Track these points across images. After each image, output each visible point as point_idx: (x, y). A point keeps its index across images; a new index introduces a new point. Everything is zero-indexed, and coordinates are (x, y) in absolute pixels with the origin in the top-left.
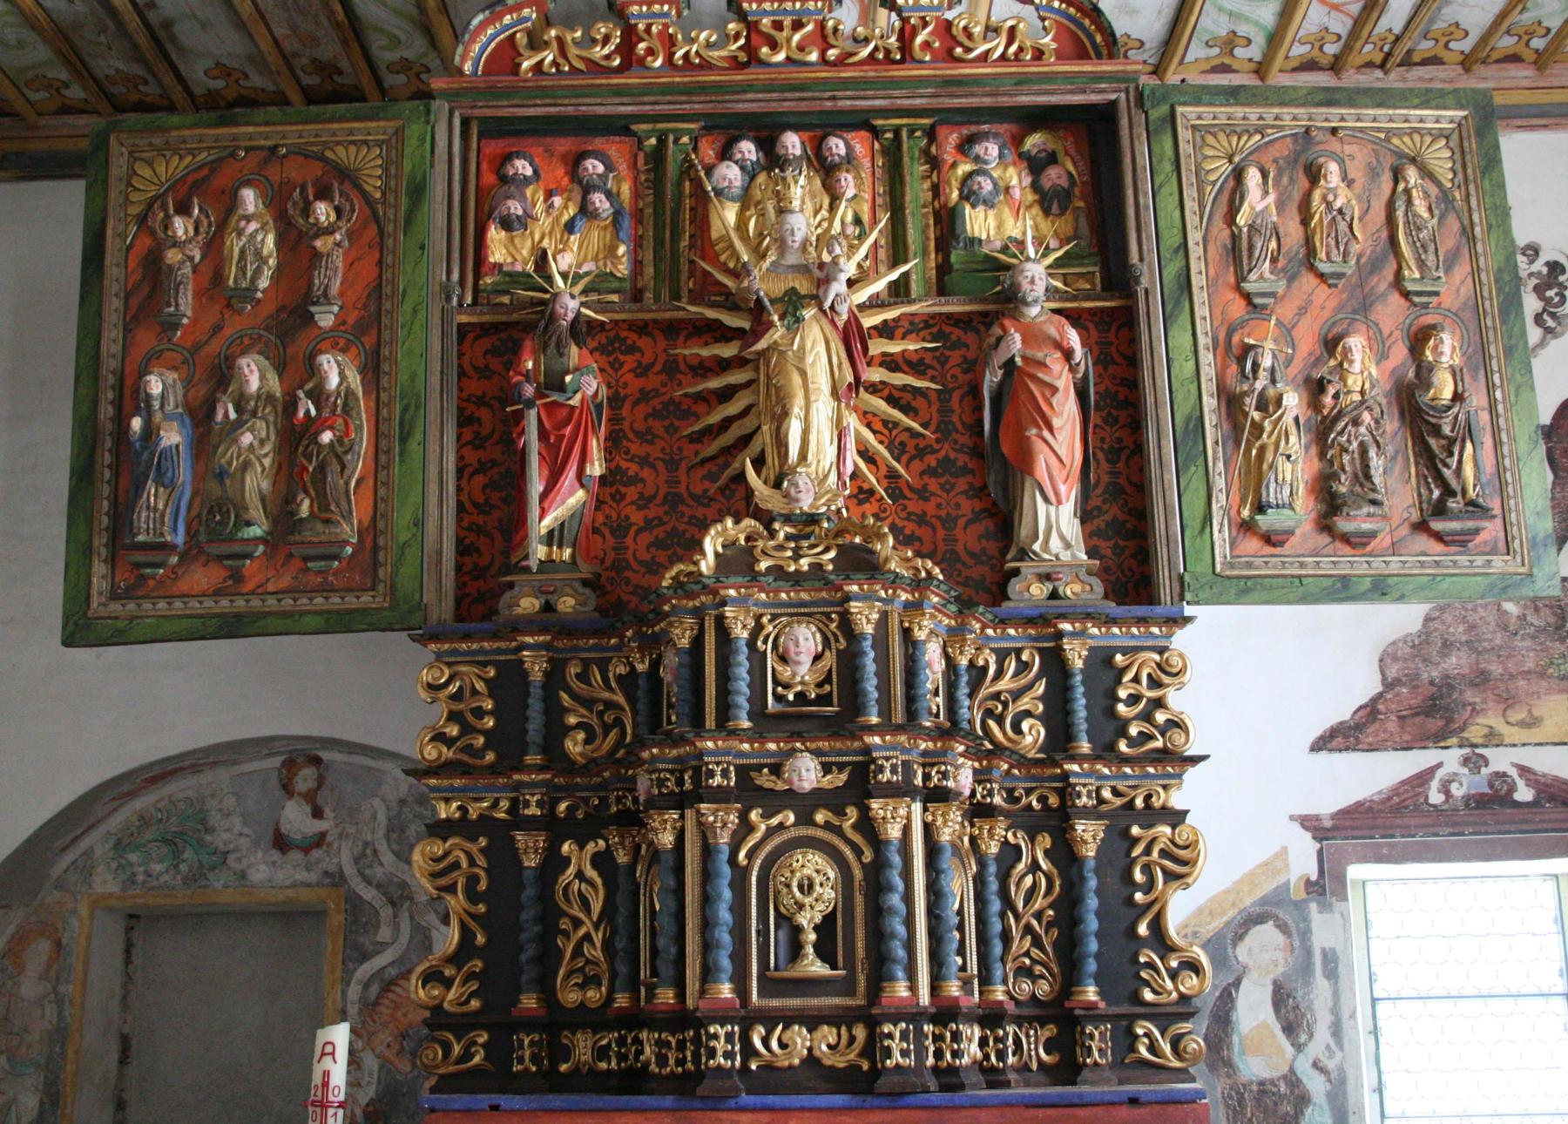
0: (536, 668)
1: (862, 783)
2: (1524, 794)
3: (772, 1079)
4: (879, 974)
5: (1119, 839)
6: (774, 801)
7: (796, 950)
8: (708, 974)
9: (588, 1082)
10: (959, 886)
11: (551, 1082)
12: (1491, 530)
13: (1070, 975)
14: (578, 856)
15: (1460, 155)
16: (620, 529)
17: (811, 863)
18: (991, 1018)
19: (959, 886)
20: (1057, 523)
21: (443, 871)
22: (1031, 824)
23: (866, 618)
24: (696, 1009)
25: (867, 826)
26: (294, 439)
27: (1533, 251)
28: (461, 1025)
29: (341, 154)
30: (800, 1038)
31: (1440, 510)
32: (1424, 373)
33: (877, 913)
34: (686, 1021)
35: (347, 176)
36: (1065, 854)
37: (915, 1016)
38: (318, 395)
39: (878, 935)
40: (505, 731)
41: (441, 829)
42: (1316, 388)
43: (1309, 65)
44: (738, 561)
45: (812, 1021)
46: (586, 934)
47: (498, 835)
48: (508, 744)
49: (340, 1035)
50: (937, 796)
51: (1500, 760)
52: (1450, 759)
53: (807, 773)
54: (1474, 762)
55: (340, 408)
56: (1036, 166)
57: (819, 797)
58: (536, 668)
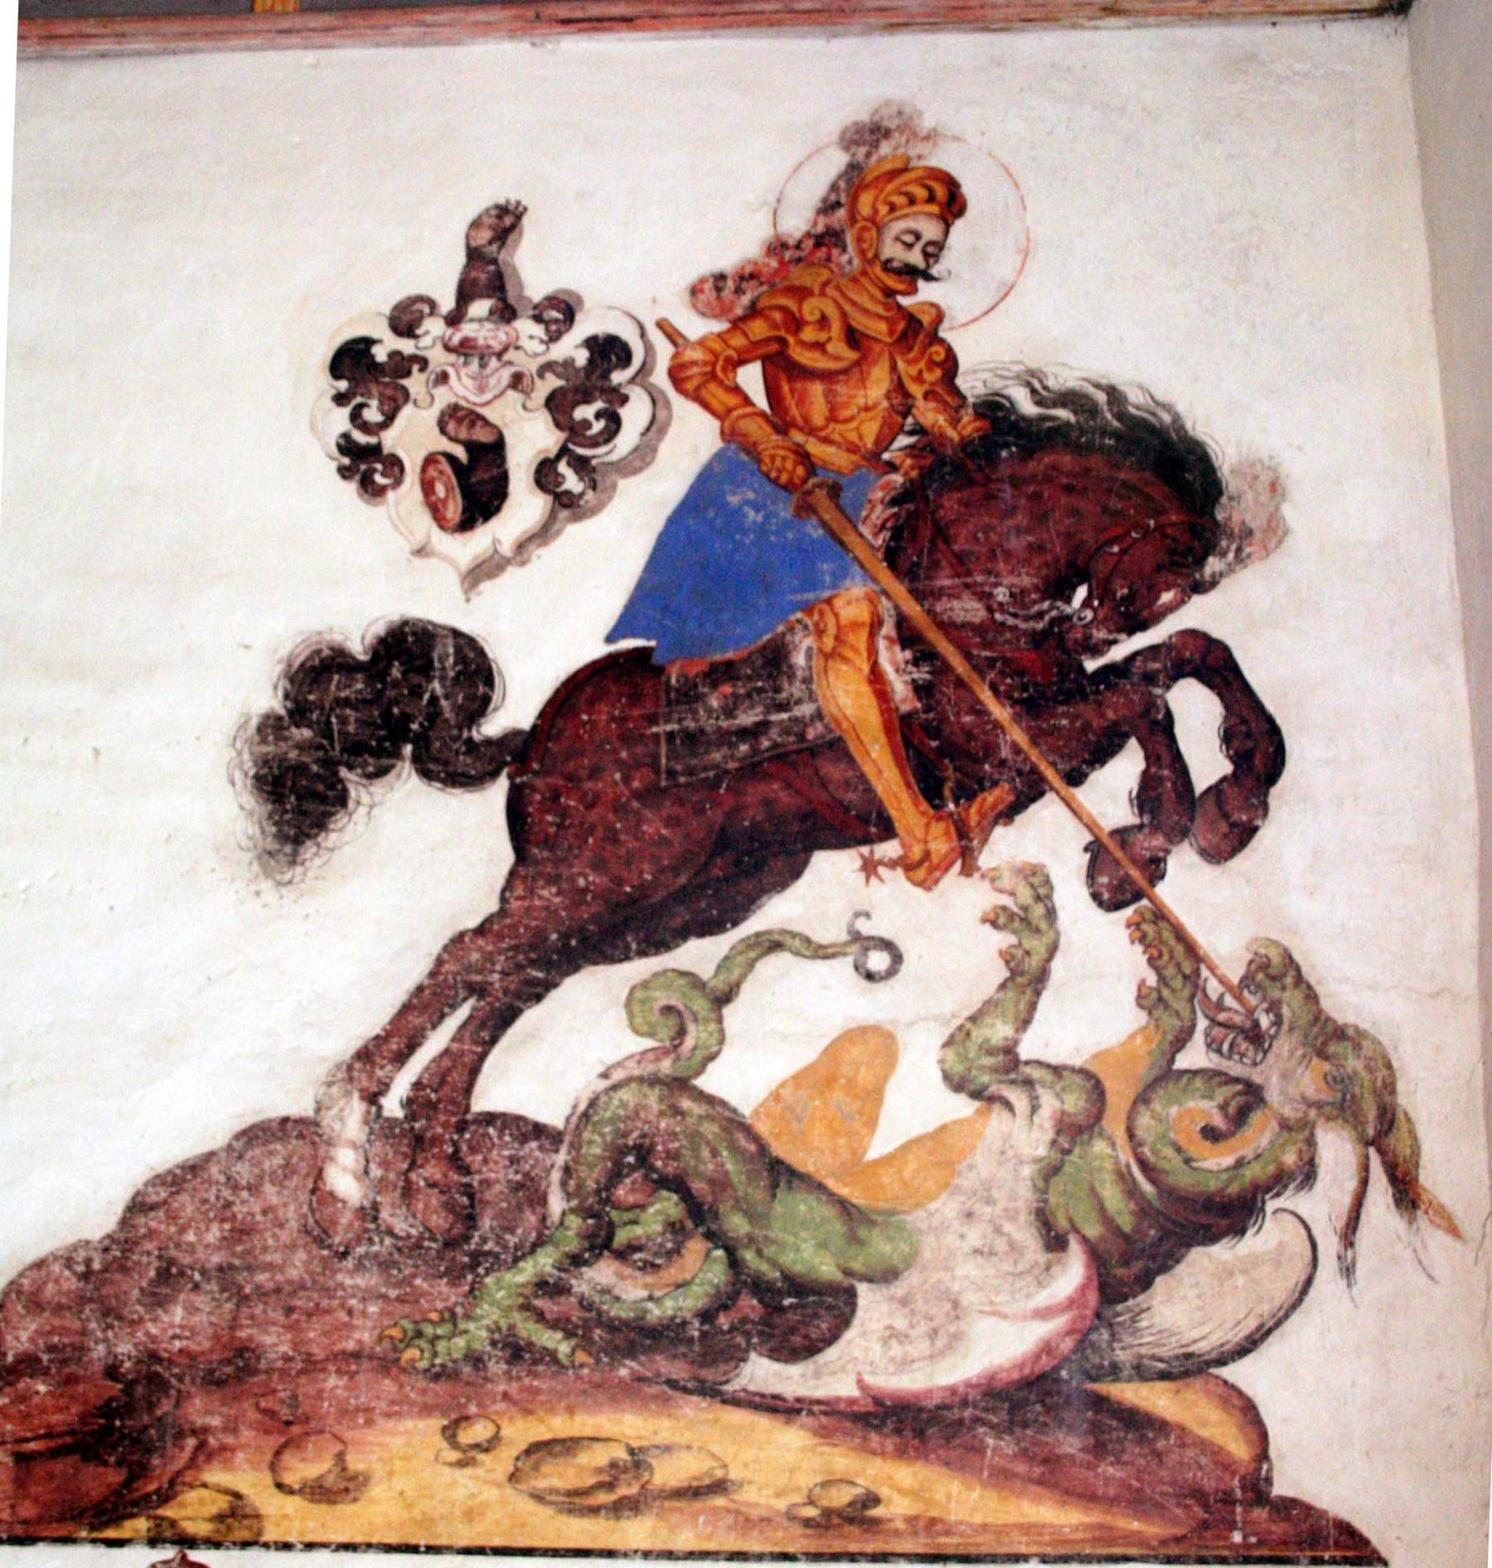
27: (562, 311)
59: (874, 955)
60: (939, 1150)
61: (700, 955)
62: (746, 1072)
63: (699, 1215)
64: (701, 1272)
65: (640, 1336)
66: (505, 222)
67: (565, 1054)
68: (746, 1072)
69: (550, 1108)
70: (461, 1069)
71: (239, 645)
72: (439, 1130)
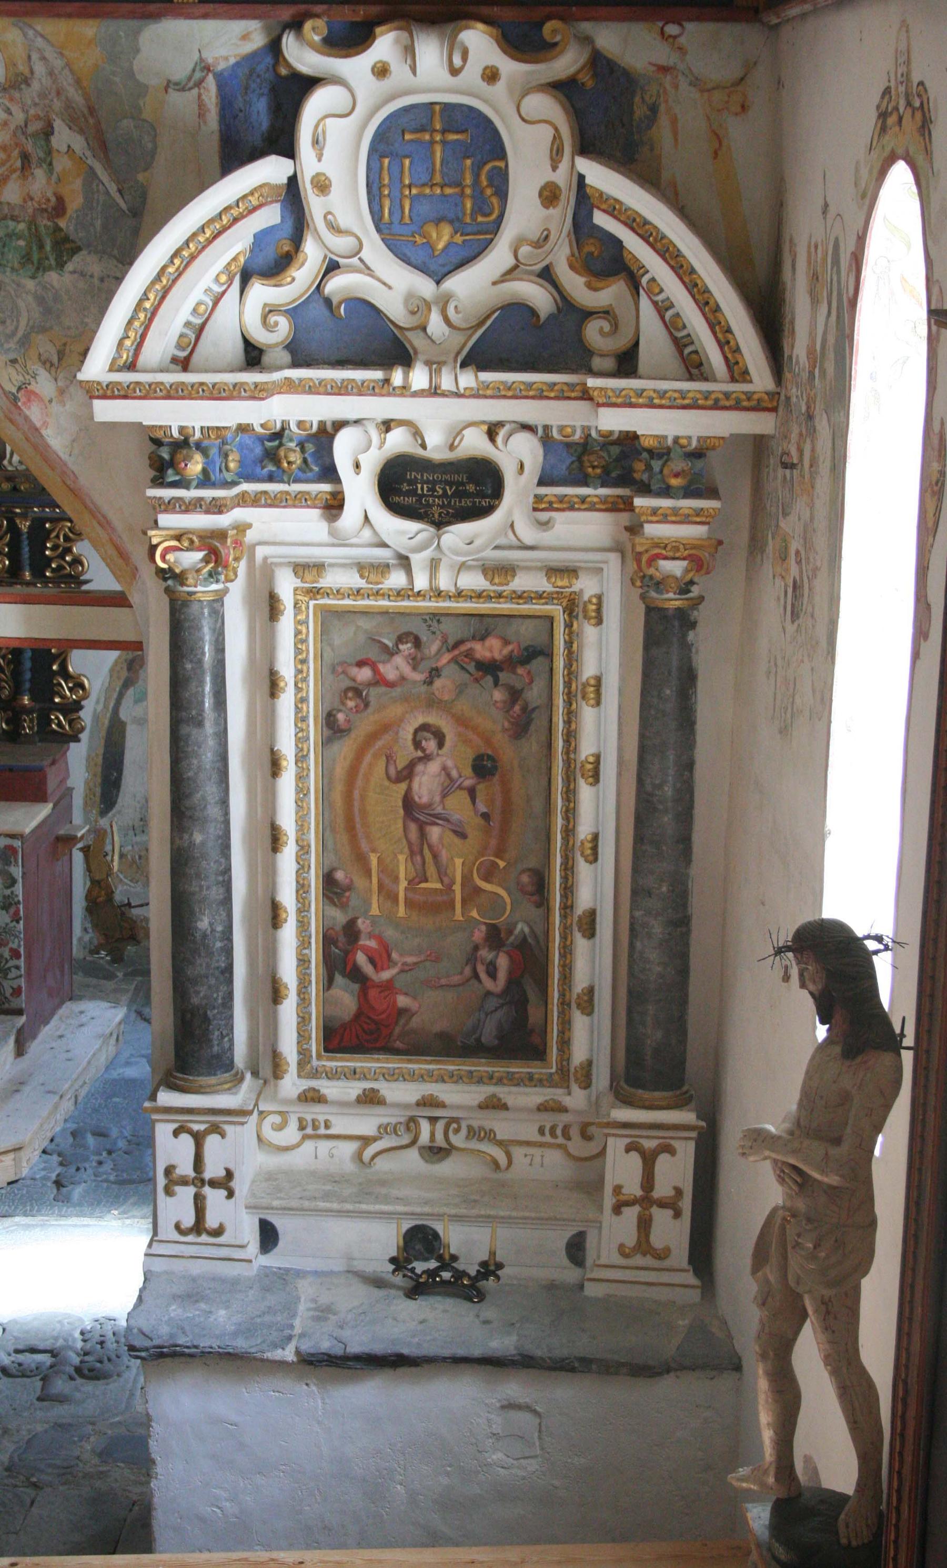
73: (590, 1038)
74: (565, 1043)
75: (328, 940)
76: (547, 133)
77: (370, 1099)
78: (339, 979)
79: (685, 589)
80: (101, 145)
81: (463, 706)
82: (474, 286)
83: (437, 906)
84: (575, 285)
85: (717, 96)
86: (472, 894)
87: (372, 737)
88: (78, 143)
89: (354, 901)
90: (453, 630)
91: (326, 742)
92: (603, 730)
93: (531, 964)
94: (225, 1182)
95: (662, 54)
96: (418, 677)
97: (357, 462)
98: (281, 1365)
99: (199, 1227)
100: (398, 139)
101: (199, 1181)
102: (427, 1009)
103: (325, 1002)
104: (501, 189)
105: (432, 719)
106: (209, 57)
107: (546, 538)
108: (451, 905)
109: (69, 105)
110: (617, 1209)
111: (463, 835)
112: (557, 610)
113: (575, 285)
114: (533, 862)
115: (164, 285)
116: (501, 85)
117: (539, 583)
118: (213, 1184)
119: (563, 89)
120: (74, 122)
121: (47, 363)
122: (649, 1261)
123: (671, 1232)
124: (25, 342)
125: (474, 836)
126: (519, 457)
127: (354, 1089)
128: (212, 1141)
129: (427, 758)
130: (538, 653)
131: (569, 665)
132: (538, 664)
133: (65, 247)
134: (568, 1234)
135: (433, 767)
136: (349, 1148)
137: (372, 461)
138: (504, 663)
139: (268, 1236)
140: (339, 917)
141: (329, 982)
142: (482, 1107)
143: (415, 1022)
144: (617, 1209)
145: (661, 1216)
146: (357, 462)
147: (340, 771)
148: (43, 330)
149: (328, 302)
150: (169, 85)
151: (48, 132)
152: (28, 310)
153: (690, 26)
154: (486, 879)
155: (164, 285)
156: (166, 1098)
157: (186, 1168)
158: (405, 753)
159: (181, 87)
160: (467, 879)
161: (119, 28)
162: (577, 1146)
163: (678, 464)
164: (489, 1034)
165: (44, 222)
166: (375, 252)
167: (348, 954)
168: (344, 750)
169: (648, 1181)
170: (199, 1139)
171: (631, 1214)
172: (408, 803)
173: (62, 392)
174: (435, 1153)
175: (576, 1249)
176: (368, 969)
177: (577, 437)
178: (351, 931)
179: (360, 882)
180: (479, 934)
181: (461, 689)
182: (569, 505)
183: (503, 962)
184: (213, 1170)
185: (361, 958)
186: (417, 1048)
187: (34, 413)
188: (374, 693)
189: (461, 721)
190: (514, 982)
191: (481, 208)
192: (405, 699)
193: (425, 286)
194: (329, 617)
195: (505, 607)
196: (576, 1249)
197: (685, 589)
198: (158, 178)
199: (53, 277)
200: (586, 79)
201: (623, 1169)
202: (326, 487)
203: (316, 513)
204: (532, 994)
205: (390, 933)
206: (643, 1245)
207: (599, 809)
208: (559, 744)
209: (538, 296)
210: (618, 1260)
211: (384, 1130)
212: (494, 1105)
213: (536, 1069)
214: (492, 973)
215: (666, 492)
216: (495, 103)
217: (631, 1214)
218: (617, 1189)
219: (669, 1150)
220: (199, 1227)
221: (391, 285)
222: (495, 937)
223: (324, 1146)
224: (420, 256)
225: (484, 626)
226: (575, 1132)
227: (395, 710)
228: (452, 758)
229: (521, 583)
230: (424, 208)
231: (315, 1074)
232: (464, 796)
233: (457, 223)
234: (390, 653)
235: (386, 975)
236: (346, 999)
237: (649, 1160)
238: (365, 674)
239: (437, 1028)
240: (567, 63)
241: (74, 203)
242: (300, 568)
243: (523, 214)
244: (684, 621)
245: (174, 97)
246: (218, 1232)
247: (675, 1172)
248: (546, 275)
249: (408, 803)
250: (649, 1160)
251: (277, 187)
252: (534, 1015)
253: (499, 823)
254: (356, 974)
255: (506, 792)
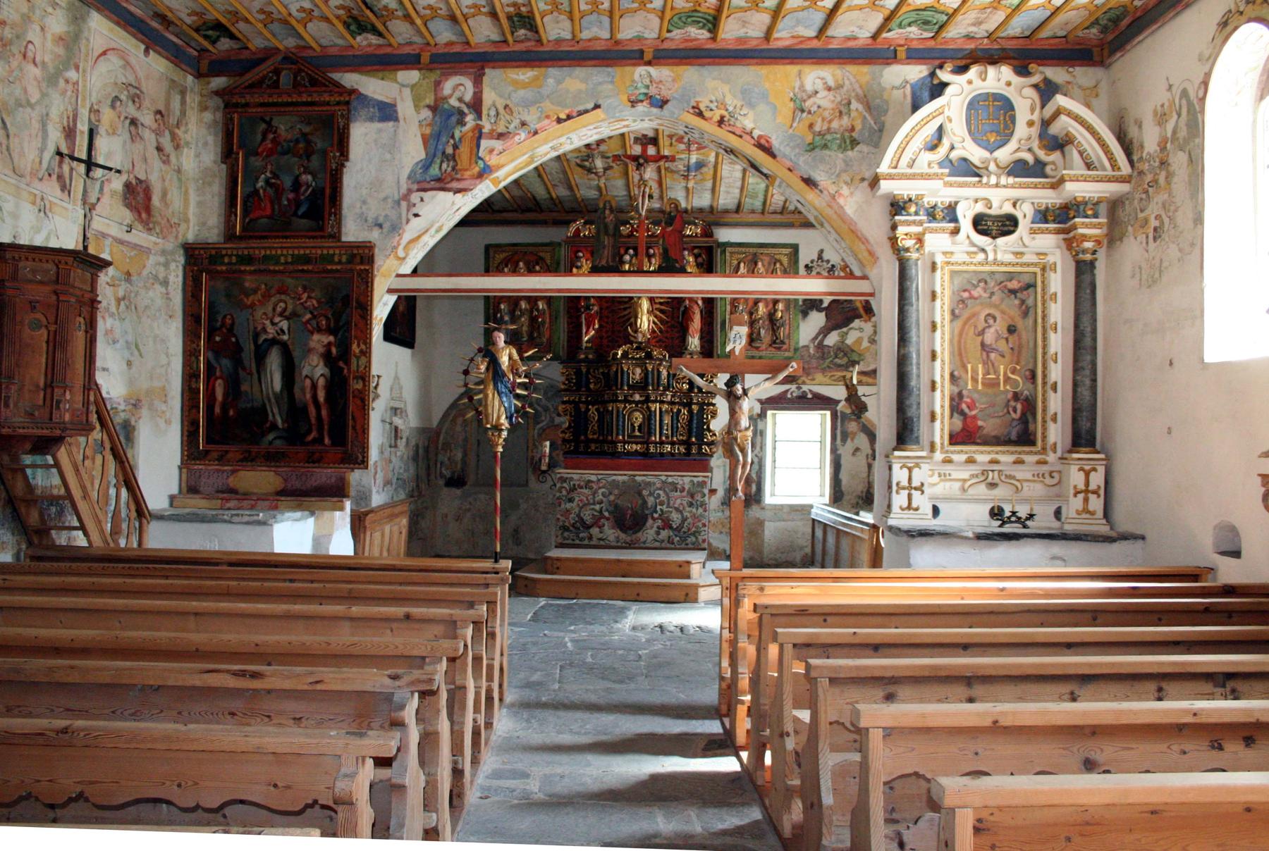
0: (584, 370)
1: (647, 400)
2: (810, 396)
3: (629, 453)
4: (650, 434)
5: (701, 410)
6: (631, 402)
7: (633, 430)
8: (618, 434)
9: (593, 453)
10: (667, 420)
11: (586, 453)
12: (785, 347)
13: (690, 437)
14: (592, 409)
15: (790, 260)
16: (601, 338)
17: (637, 414)
18: (673, 444)
19: (667, 420)
20: (694, 342)
21: (565, 411)
22: (684, 405)
23: (650, 368)
24: (453, 473)
25: (648, 408)
26: (533, 320)
27: (828, 261)
28: (568, 441)
29: (542, 254)
30: (634, 446)
31: (774, 342)
32: (776, 311)
33: (649, 424)
34: (614, 443)
35: (543, 259)
36: (690, 411)
37: (656, 443)
38: (538, 310)
39: (649, 428)
40: (577, 382)
41: (564, 403)
42: (751, 314)
43: (775, 212)
44: (625, 355)
45: (637, 443)
46: (593, 425)
47: (576, 404)
48: (578, 385)
49: (548, 443)
50: (662, 402)
51: (805, 388)
52: (793, 387)
53: (637, 397)
54: (799, 388)
55: (542, 313)
56: (696, 257)
57: (639, 402)
58: (584, 370)
59: (861, 330)
60: (867, 349)
61: (845, 330)
62: (849, 341)
63: (845, 355)
64: (846, 360)
65: (840, 366)
66: (822, 251)
67: (832, 339)
68: (849, 341)
69: (831, 344)
70: (822, 341)
71: (853, 454)
72: (820, 346)
73: (1057, 433)
74: (1044, 437)
75: (952, 399)
76: (1029, 102)
77: (971, 461)
78: (955, 415)
79: (1094, 252)
80: (868, 107)
81: (1003, 306)
82: (1005, 154)
83: (995, 384)
84: (1042, 154)
85: (1088, 92)
86: (1007, 379)
87: (969, 319)
88: (860, 107)
89: (961, 383)
90: (999, 278)
91: (952, 321)
92: (1059, 312)
93: (1029, 406)
94: (920, 489)
95: (1068, 78)
96: (986, 295)
97: (965, 215)
98: (966, 538)
99: (909, 507)
100: (975, 105)
101: (910, 487)
102: (989, 426)
103: (951, 424)
104: (1013, 120)
105: (992, 311)
106: (908, 78)
107: (1033, 245)
108: (999, 384)
109: (857, 95)
110: (1075, 495)
111: (1003, 356)
112: (1037, 270)
113: (1042, 154)
114: (1030, 366)
115: (902, 150)
116: (1012, 88)
117: (1034, 259)
118: (916, 489)
119: (1036, 86)
120: (859, 100)
121: (846, 183)
122: (1088, 516)
123: (1096, 504)
124: (838, 176)
125: (1008, 356)
126: (1025, 214)
127: (964, 457)
128: (916, 472)
129: (989, 327)
130: (1031, 286)
131: (1043, 290)
132: (1031, 290)
133: (854, 143)
134: (1054, 508)
135: (992, 330)
136: (958, 485)
137: (970, 215)
138: (1022, 290)
139: (936, 511)
140: (956, 390)
141: (952, 416)
142: (1015, 463)
143: (985, 432)
144: (1075, 495)
145: (1092, 497)
146: (965, 215)
147: (956, 332)
148: (845, 171)
149: (951, 161)
150: (893, 88)
151: (849, 103)
152: (840, 165)
153: (1078, 69)
154: (1013, 373)
155: (902, 150)
156: (897, 453)
157: (905, 483)
158: (981, 325)
159: (897, 88)
160: (1005, 374)
161: (876, 68)
162: (1048, 481)
163: (1090, 206)
164: (1014, 437)
165: (847, 134)
166: (969, 143)
167: (959, 404)
168: (958, 323)
169: (1087, 483)
170: (910, 470)
171: (1081, 496)
172: (983, 345)
173: (852, 193)
174: (993, 485)
175: (1058, 514)
176: (966, 410)
177: (1043, 207)
178: (960, 395)
179: (963, 375)
180: (1010, 396)
181: (1002, 300)
182: (1042, 232)
183: (1019, 407)
184: (915, 483)
185: (964, 406)
186: (986, 443)
187: (841, 201)
188: (969, 302)
189: (1003, 312)
190: (1023, 414)
191: (1006, 127)
192: (981, 304)
193: (986, 154)
194: (953, 273)
195: (1018, 269)
196: (1058, 514)
197: (1094, 252)
198: (888, 119)
199: (850, 153)
200: (1042, 85)
201: (1077, 478)
202: (952, 225)
203: (947, 235)
204: (1030, 419)
205: (975, 396)
206: (1086, 510)
207: (1059, 342)
208: (1040, 320)
209: (1029, 158)
210: (1075, 515)
211: (972, 476)
212: (1019, 462)
213: (1032, 449)
214: (1015, 411)
215: (1087, 217)
216: (1010, 93)
217: (1081, 496)
218: (1075, 487)
219: (1094, 470)
220: (909, 507)
221: (976, 154)
222: (1016, 396)
223: (948, 484)
224: (985, 144)
225: (1011, 276)
226: (1047, 475)
227: (978, 308)
228: (1000, 326)
229: (1026, 259)
230: (987, 128)
231: (947, 452)
232: (1004, 342)
233: (998, 133)
234: (975, 287)
235: (973, 413)
236: (958, 423)
237: (1087, 474)
238: (966, 295)
239: (993, 434)
240: (1036, 79)
241: (858, 127)
242: (945, 253)
243: (1021, 130)
244: (1092, 264)
245: (895, 92)
246: (917, 509)
247: (1097, 479)
248: (1030, 150)
249: (983, 345)
250: (1087, 474)
251: (328, 549)
252: (1031, 427)
253: (1017, 352)
254: (962, 413)
255: (1020, 338)
